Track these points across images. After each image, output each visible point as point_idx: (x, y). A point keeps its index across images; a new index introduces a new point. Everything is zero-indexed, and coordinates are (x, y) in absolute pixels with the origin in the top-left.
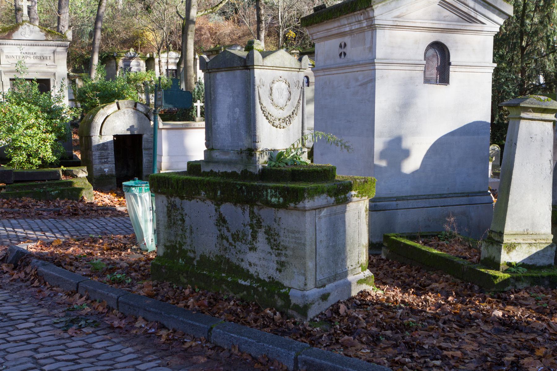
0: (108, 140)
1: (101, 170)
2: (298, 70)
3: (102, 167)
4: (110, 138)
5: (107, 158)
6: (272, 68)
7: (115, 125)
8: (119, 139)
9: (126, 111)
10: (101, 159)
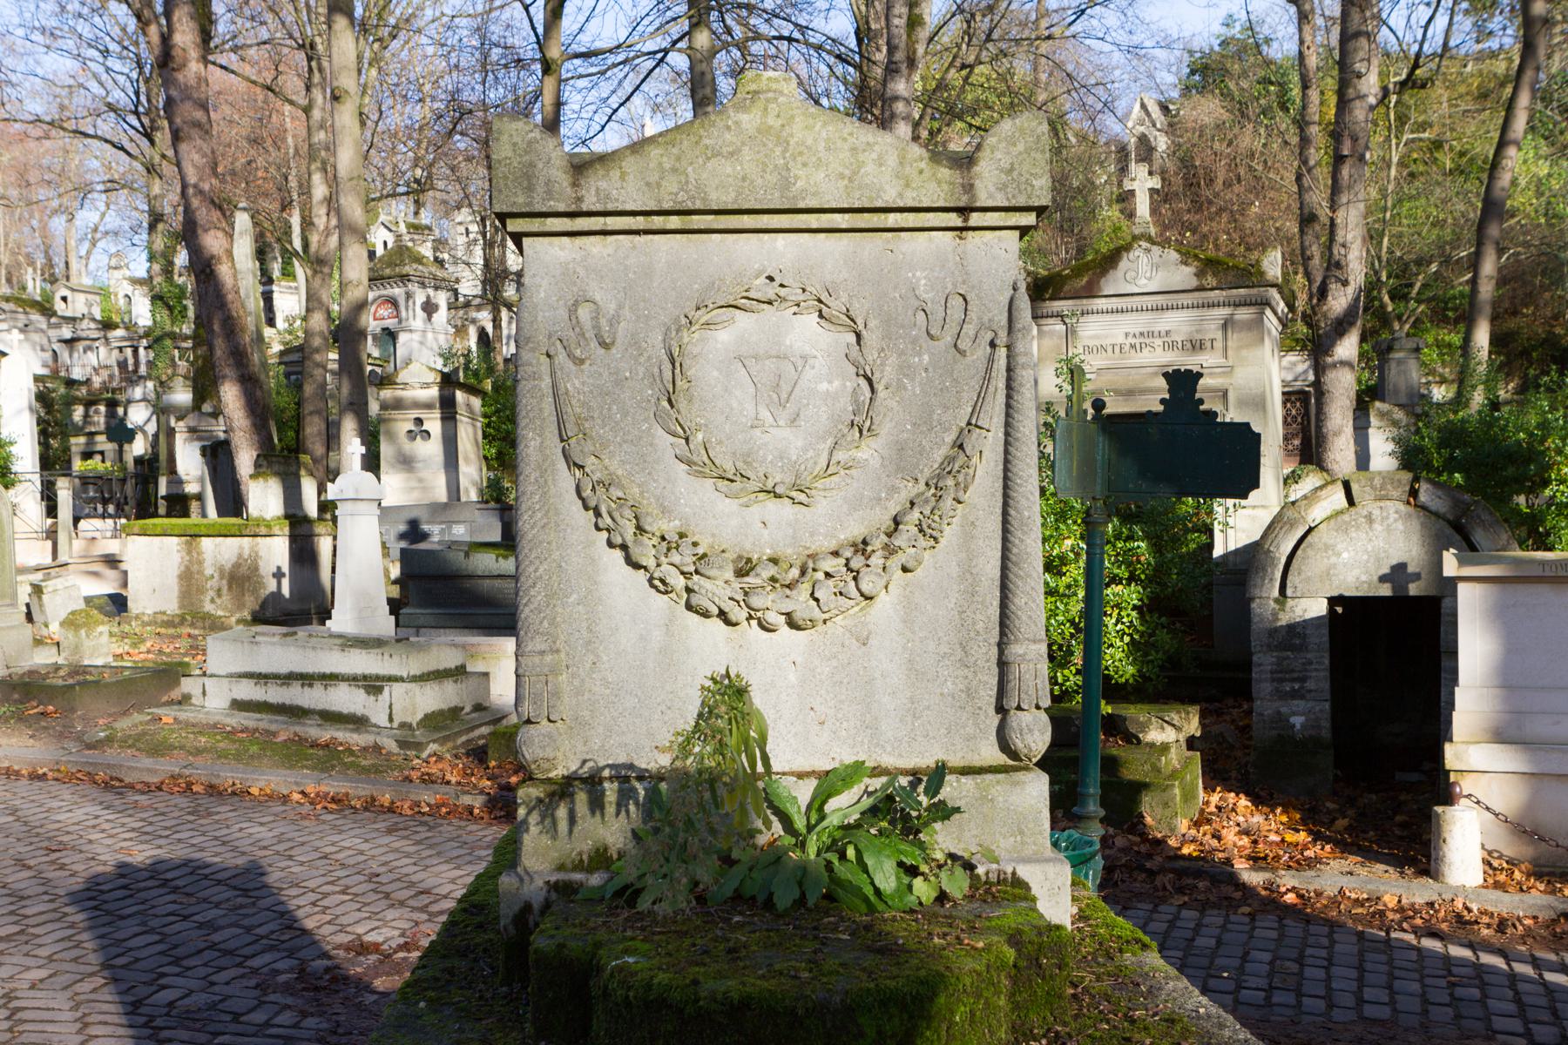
0: (1308, 616)
1: (1281, 720)
2: (954, 219)
3: (1284, 710)
4: (1316, 608)
5: (1303, 680)
6: (674, 222)
7: (1333, 560)
8: (1349, 613)
9: (1376, 512)
10: (1281, 680)
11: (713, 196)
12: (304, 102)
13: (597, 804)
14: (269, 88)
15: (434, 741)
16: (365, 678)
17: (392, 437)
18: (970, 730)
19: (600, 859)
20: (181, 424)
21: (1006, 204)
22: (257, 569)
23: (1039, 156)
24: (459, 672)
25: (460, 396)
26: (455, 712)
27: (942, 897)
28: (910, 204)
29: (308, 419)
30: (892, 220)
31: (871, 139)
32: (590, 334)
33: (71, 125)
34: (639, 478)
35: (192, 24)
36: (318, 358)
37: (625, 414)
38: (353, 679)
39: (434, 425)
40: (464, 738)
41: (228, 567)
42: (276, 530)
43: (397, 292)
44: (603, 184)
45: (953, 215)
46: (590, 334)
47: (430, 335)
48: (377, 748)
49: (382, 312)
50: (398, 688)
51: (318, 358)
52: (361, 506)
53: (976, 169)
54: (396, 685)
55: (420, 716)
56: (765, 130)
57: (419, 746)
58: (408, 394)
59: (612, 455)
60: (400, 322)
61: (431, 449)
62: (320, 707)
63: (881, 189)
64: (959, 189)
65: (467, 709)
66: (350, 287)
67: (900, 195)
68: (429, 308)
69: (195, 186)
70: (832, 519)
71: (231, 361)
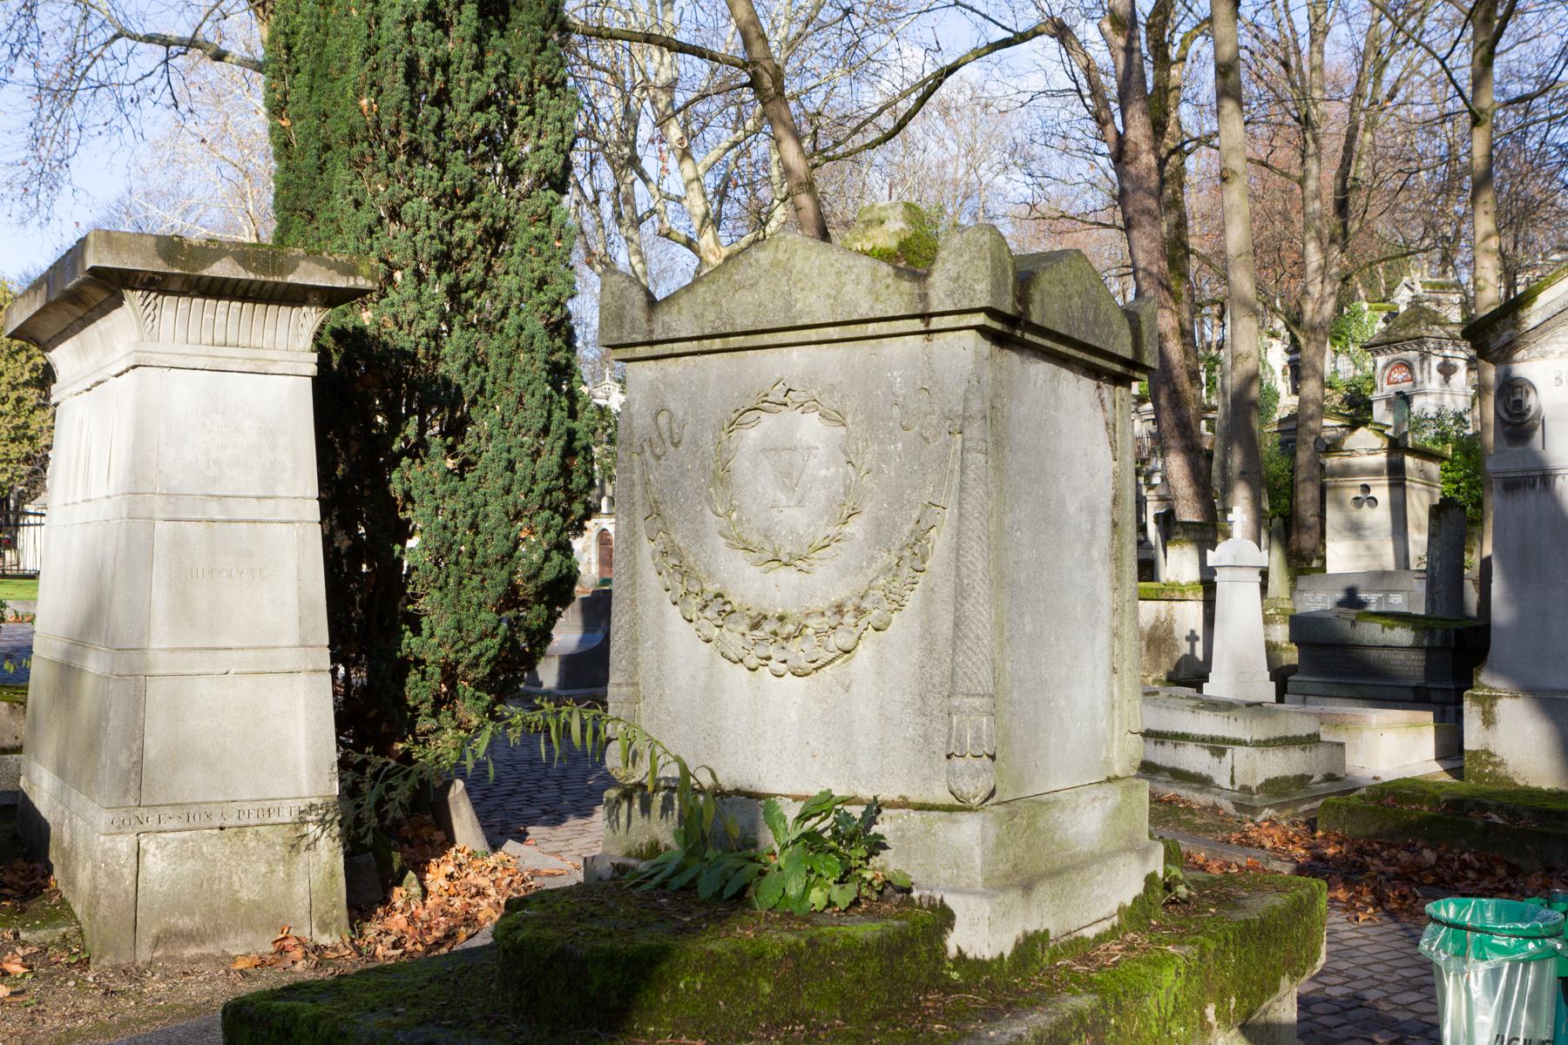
2: (918, 325)
6: (717, 344)
11: (739, 321)
12: (1299, 174)
13: (646, 809)
14: (1264, 164)
15: (1270, 807)
16: (1212, 739)
17: (1340, 503)
18: (926, 771)
19: (654, 849)
20: (1152, 493)
21: (952, 308)
22: (1172, 632)
23: (980, 263)
24: (1312, 740)
25: (1410, 461)
26: (1302, 780)
27: (830, 904)
28: (879, 315)
29: (1301, 487)
30: (871, 329)
31: (851, 263)
32: (666, 436)
33: (1091, 218)
34: (694, 549)
35: (1144, 119)
36: (1312, 425)
37: (687, 499)
38: (1201, 740)
39: (1381, 492)
40: (1306, 807)
41: (1147, 628)
42: (1189, 595)
43: (1412, 355)
44: (666, 318)
45: (918, 321)
46: (666, 436)
47: (1447, 398)
48: (1215, 809)
49: (1398, 376)
50: (1240, 752)
51: (1312, 425)
52: (1242, 573)
53: (931, 280)
54: (1238, 748)
55: (1260, 780)
56: (775, 264)
57: (1254, 810)
58: (1356, 461)
59: (677, 531)
60: (1415, 385)
61: (1379, 516)
62: (1170, 765)
63: (858, 305)
64: (917, 299)
65: (1317, 778)
66: (1240, 360)
67: (872, 308)
68: (1447, 370)
69: (1145, 270)
70: (823, 583)
71: (1176, 433)
